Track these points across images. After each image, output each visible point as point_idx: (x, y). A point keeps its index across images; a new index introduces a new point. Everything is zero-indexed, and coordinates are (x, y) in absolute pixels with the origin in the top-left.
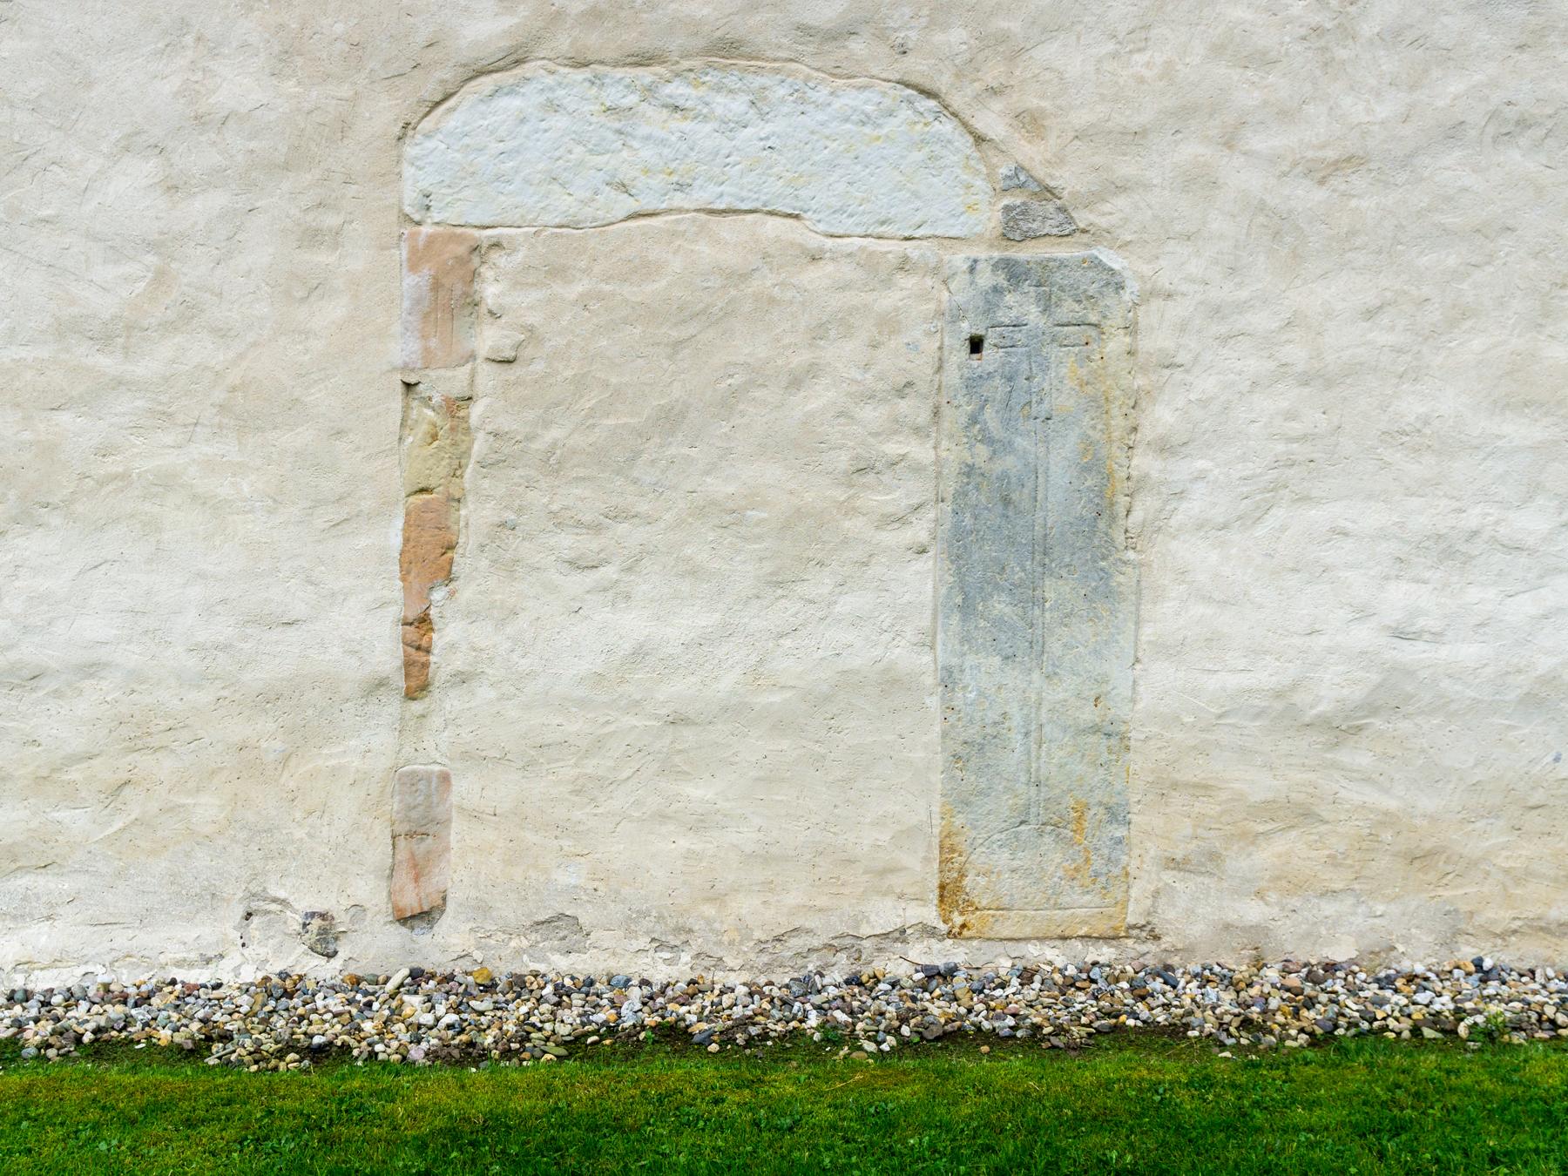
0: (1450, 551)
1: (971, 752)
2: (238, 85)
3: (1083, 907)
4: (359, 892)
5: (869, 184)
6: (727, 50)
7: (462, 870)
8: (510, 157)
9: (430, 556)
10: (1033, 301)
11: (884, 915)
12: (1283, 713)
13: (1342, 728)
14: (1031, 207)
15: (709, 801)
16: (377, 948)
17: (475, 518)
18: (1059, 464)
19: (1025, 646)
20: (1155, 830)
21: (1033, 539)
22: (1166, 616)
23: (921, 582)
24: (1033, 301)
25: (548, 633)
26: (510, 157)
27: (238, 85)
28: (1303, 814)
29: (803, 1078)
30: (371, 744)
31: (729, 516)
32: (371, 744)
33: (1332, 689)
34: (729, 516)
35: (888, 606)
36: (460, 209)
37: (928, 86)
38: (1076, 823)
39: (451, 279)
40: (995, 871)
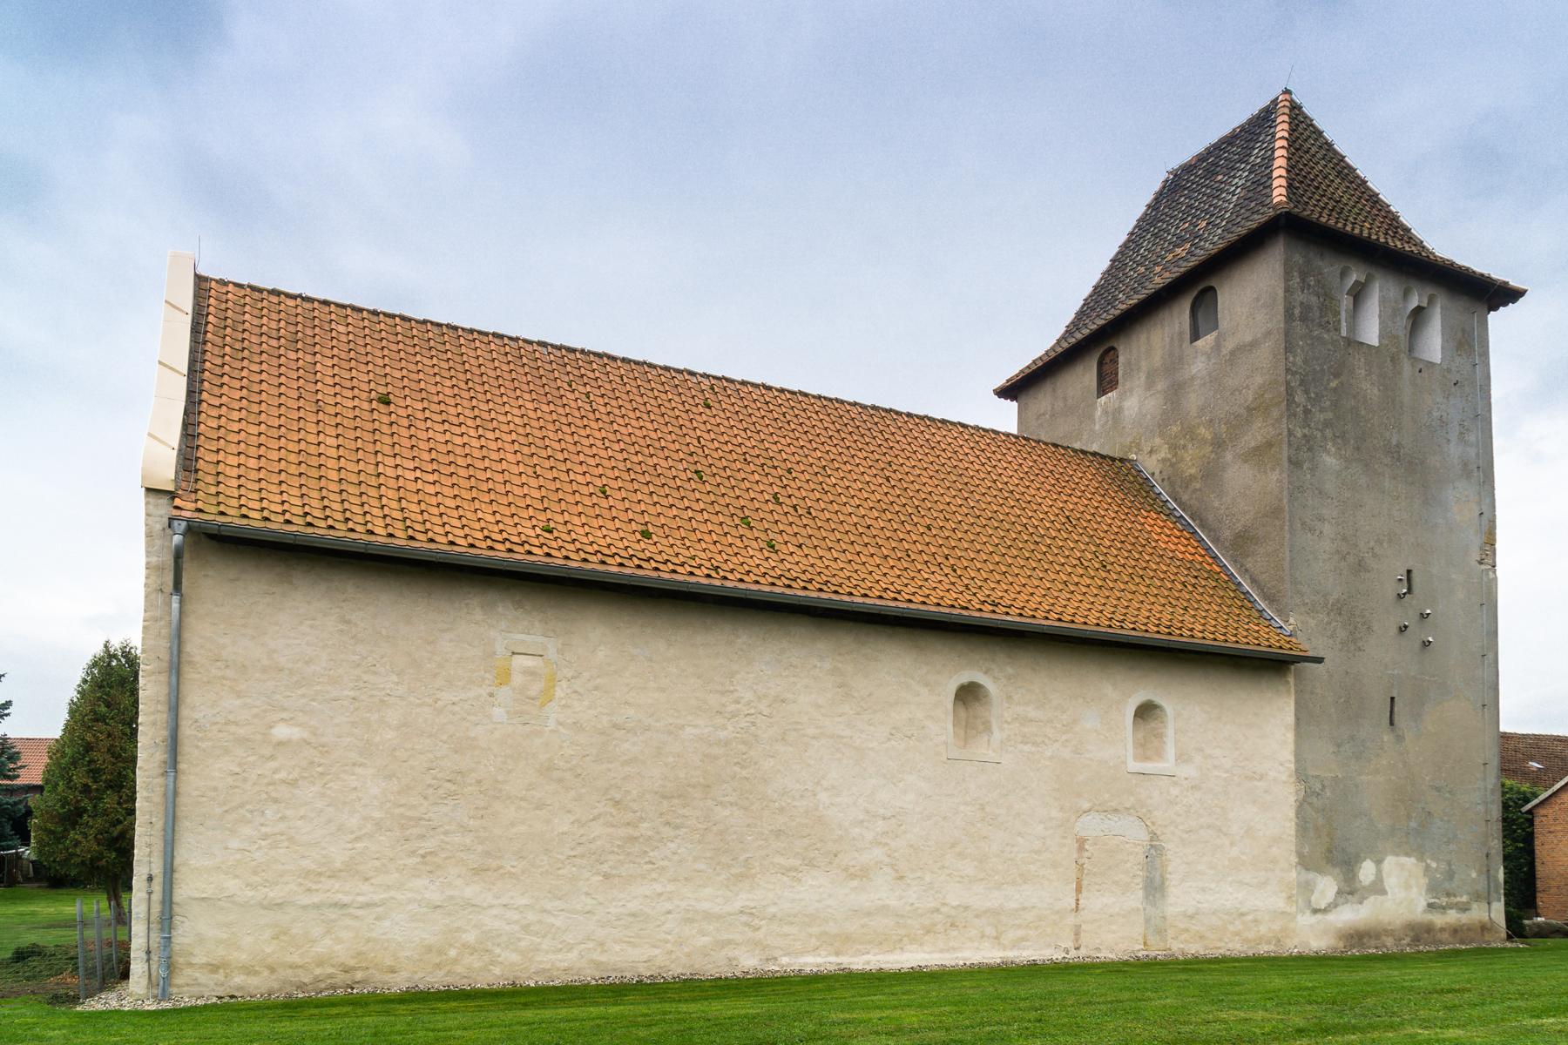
0: (1203, 890)
1: (1147, 921)
2: (1054, 813)
3: (1162, 945)
4: (1070, 944)
5: (1135, 833)
6: (1116, 810)
7: (1084, 940)
8: (1090, 826)
9: (1079, 890)
10: (1154, 852)
11: (1138, 947)
12: (1184, 914)
13: (1191, 917)
14: (1154, 836)
15: (1113, 929)
16: (1073, 954)
17: (1085, 883)
18: (1158, 879)
19: (1154, 904)
20: (1171, 933)
21: (1154, 888)
22: (1171, 899)
23: (1141, 893)
24: (1154, 852)
25: (1095, 902)
26: (1090, 826)
27: (1054, 813)
28: (1187, 930)
29: (376, 716)
30: (1071, 920)
31: (1116, 883)
32: (1071, 920)
33: (1191, 911)
34: (1116, 883)
35: (1135, 899)
36: (1083, 834)
37: (187, 749)
38: (1160, 932)
39: (1081, 843)
40: (1152, 940)
